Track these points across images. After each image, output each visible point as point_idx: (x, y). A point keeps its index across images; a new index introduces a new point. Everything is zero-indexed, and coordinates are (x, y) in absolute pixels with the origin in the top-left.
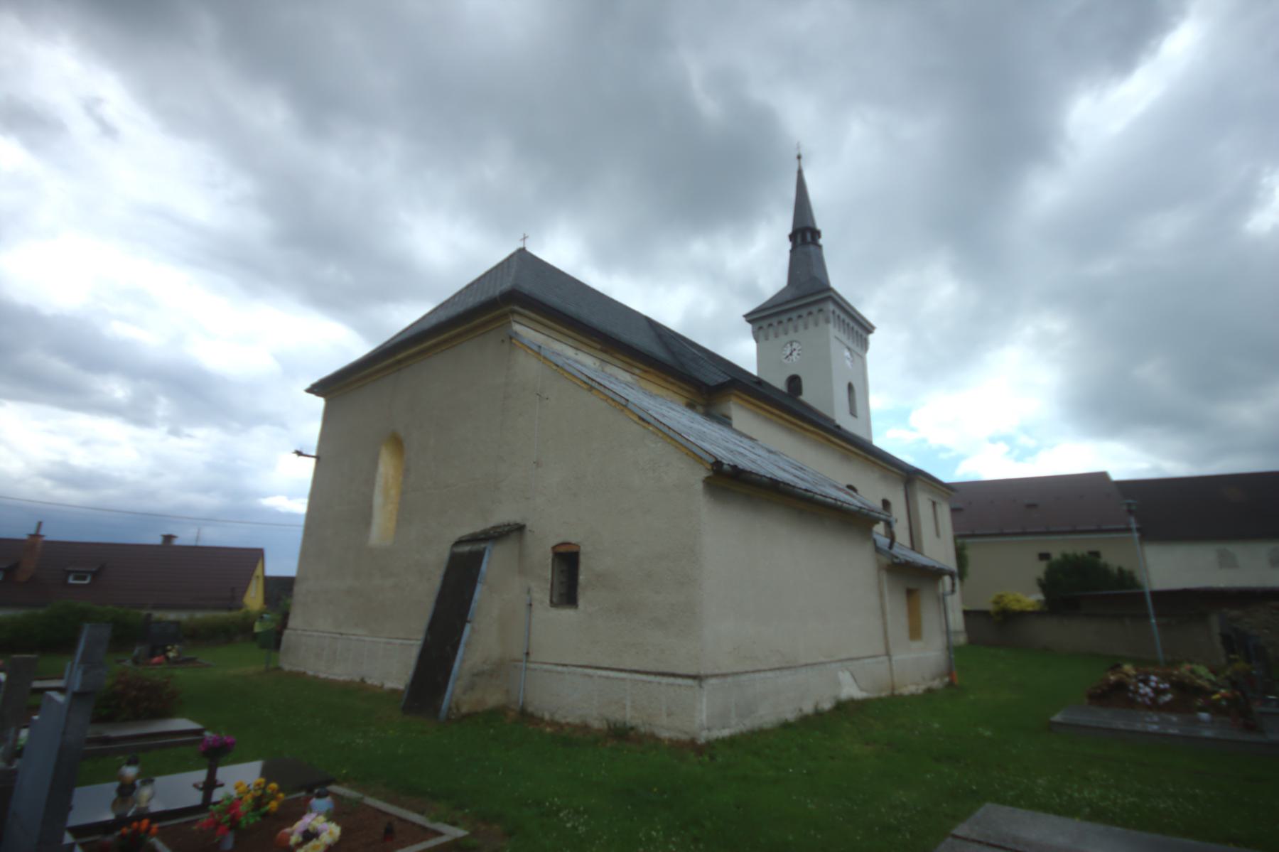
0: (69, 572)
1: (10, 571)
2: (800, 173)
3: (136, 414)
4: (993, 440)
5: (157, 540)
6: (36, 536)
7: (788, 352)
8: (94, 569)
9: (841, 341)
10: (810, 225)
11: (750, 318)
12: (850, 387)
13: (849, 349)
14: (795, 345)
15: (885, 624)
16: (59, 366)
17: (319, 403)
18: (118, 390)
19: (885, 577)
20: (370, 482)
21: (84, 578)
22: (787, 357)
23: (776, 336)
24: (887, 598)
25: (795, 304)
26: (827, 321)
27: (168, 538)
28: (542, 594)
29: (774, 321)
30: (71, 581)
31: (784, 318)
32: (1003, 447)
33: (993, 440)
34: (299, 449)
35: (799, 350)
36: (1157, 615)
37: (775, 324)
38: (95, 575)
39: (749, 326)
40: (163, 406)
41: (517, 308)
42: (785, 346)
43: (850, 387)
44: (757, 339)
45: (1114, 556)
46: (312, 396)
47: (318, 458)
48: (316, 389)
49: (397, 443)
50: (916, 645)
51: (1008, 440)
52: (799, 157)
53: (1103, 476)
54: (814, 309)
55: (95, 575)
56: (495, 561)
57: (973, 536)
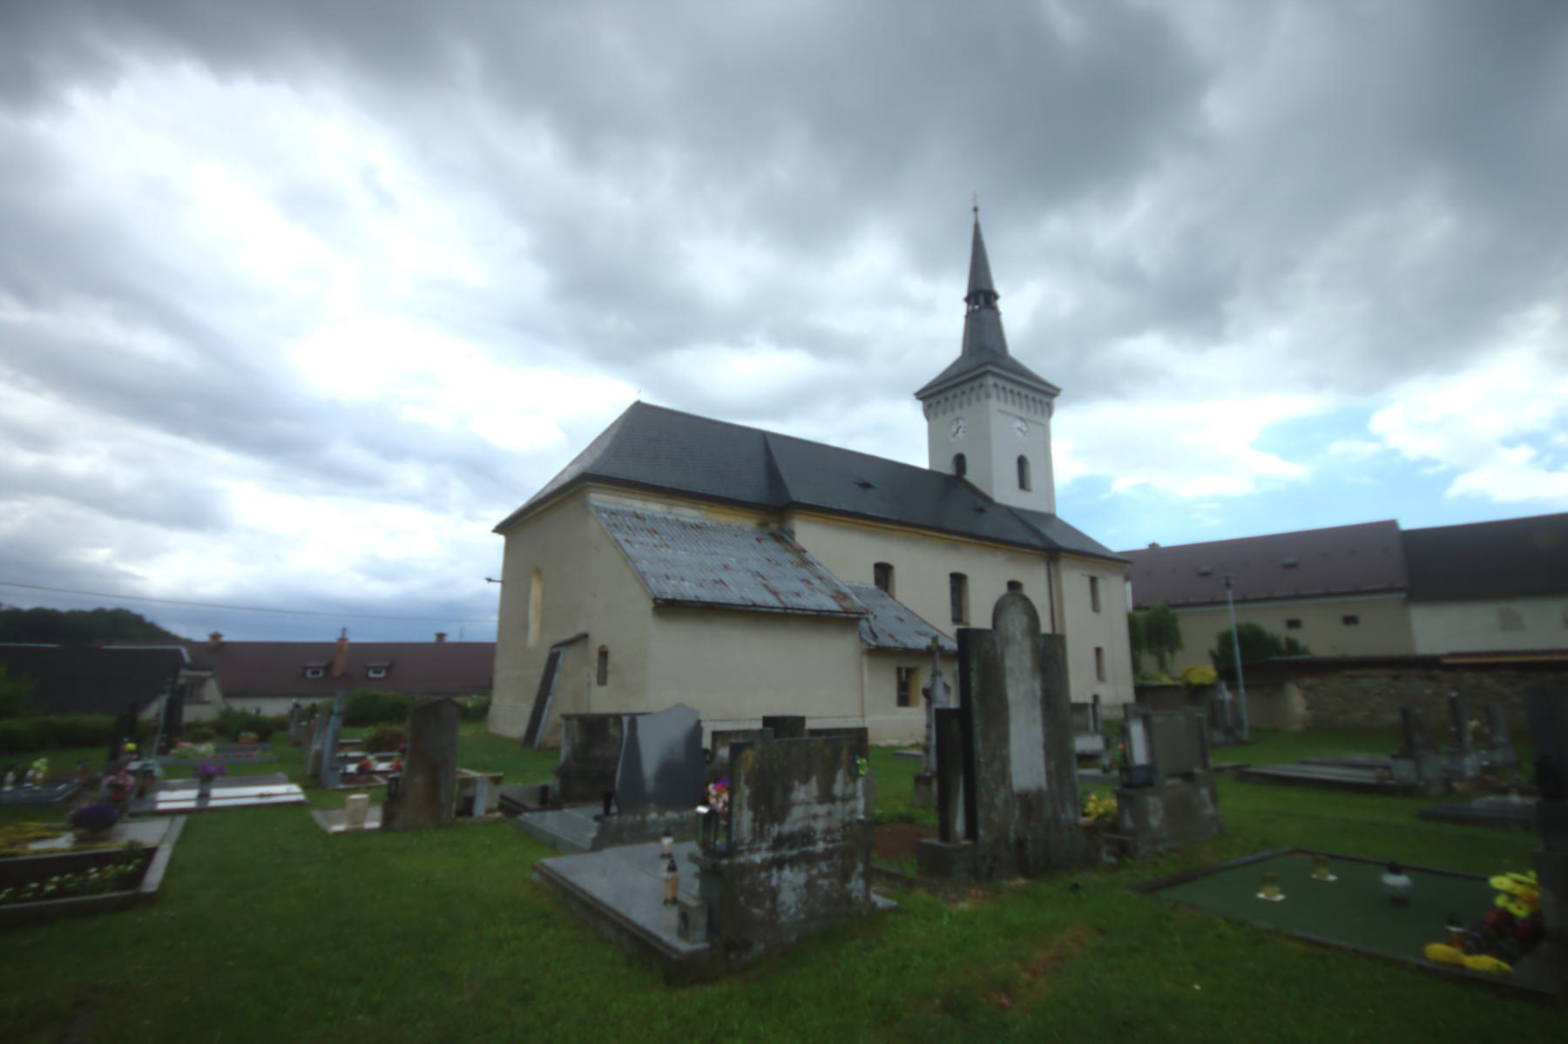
0: (368, 668)
1: (328, 668)
2: (977, 227)
3: (432, 500)
4: (1509, 443)
5: (432, 639)
6: (343, 640)
7: (955, 430)
8: (386, 664)
9: (1009, 414)
10: (985, 287)
11: (919, 396)
12: (1022, 462)
13: (1022, 419)
14: (961, 423)
15: (862, 695)
16: (360, 458)
17: (500, 540)
18: (413, 476)
19: (865, 659)
20: (527, 602)
21: (380, 672)
22: (954, 435)
23: (944, 413)
24: (866, 676)
25: (966, 377)
26: (988, 396)
27: (441, 636)
28: (594, 679)
29: (941, 398)
30: (372, 675)
31: (950, 394)
32: (1525, 452)
33: (1509, 443)
34: (488, 576)
35: (965, 427)
36: (1247, 687)
37: (942, 400)
38: (388, 669)
39: (920, 404)
40: (458, 489)
41: (589, 483)
42: (952, 424)
43: (1022, 462)
44: (927, 416)
45: (1271, 622)
46: (496, 535)
47: (503, 582)
48: (500, 529)
49: (538, 572)
50: (904, 710)
51: (1534, 439)
52: (976, 210)
53: (1391, 525)
54: (975, 384)
55: (388, 669)
56: (567, 659)
57: (1187, 605)
